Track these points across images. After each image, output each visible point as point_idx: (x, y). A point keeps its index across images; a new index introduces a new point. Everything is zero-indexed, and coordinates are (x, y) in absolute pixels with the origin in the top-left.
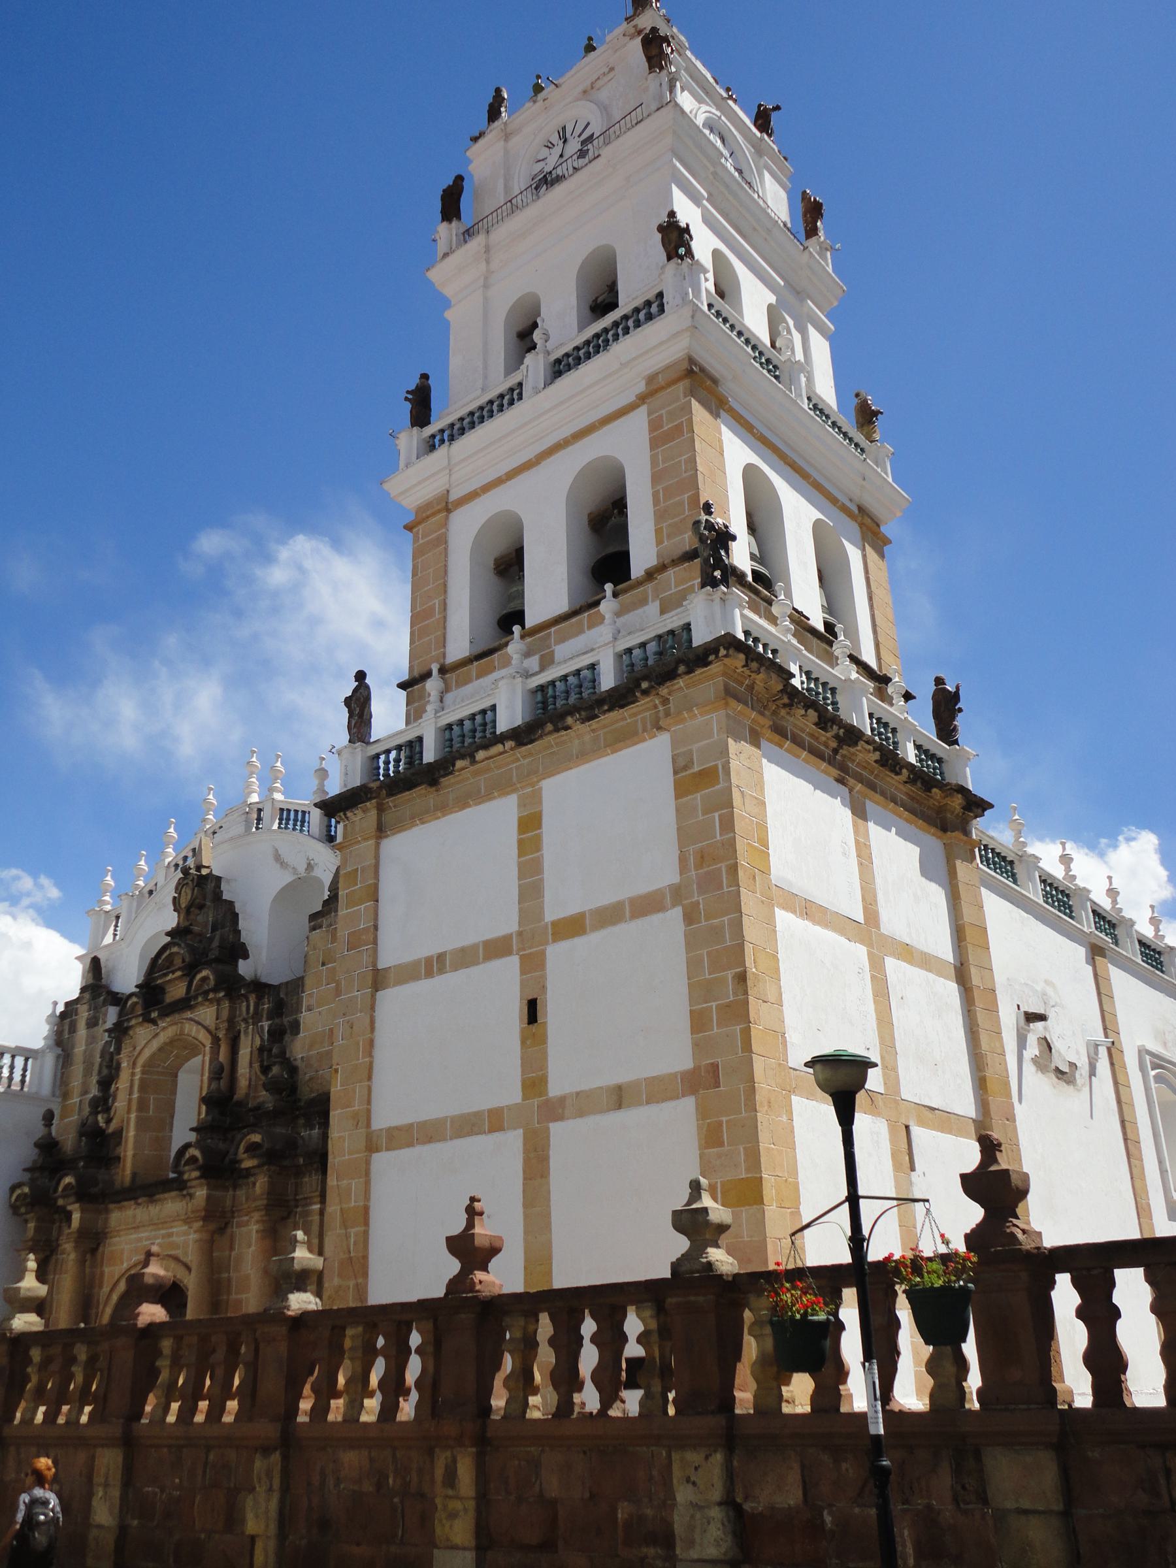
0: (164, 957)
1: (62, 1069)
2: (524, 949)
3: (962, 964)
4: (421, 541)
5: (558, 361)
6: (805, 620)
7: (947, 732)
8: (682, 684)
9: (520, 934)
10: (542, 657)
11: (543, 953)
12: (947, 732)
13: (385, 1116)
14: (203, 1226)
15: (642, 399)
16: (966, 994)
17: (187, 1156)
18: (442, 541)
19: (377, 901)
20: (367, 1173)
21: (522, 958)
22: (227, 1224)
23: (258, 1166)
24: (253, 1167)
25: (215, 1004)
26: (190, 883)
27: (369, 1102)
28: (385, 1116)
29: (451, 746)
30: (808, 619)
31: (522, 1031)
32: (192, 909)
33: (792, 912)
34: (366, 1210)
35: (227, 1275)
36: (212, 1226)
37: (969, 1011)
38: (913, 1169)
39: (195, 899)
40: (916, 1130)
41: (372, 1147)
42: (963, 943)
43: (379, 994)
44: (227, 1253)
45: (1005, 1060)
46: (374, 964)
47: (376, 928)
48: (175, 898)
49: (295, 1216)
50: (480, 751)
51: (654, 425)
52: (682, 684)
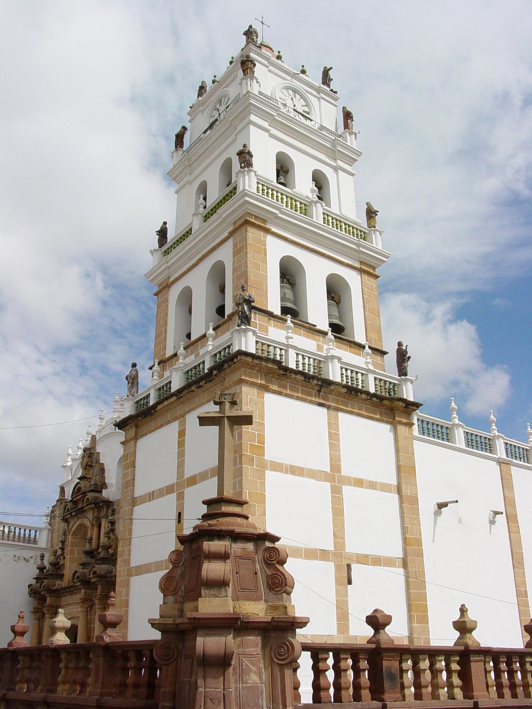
0: (76, 488)
1: (51, 535)
2: (178, 490)
3: (399, 484)
4: (160, 301)
5: (206, 216)
6: (313, 327)
7: (402, 372)
8: (228, 372)
9: (177, 483)
10: (196, 354)
11: (183, 492)
12: (402, 372)
13: (134, 563)
14: (82, 605)
15: (231, 234)
16: (400, 498)
17: (76, 576)
18: (166, 301)
19: (135, 467)
20: (128, 586)
21: (177, 494)
22: (93, 604)
23: (98, 581)
24: (96, 581)
25: (92, 509)
26: (86, 456)
27: (129, 556)
28: (134, 563)
29: (160, 398)
30: (315, 326)
31: (176, 525)
32: (87, 467)
33: (280, 472)
34: (127, 601)
35: (93, 625)
36: (86, 605)
37: (401, 506)
38: (350, 582)
39: (88, 463)
40: (353, 566)
41: (130, 575)
42: (400, 474)
43: (135, 508)
44: (93, 616)
45: (420, 529)
46: (133, 495)
47: (134, 479)
48: (81, 462)
49: (95, 605)
50: (165, 401)
51: (235, 246)
52: (228, 372)
